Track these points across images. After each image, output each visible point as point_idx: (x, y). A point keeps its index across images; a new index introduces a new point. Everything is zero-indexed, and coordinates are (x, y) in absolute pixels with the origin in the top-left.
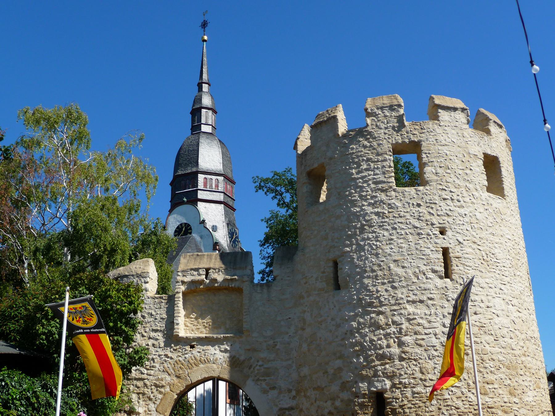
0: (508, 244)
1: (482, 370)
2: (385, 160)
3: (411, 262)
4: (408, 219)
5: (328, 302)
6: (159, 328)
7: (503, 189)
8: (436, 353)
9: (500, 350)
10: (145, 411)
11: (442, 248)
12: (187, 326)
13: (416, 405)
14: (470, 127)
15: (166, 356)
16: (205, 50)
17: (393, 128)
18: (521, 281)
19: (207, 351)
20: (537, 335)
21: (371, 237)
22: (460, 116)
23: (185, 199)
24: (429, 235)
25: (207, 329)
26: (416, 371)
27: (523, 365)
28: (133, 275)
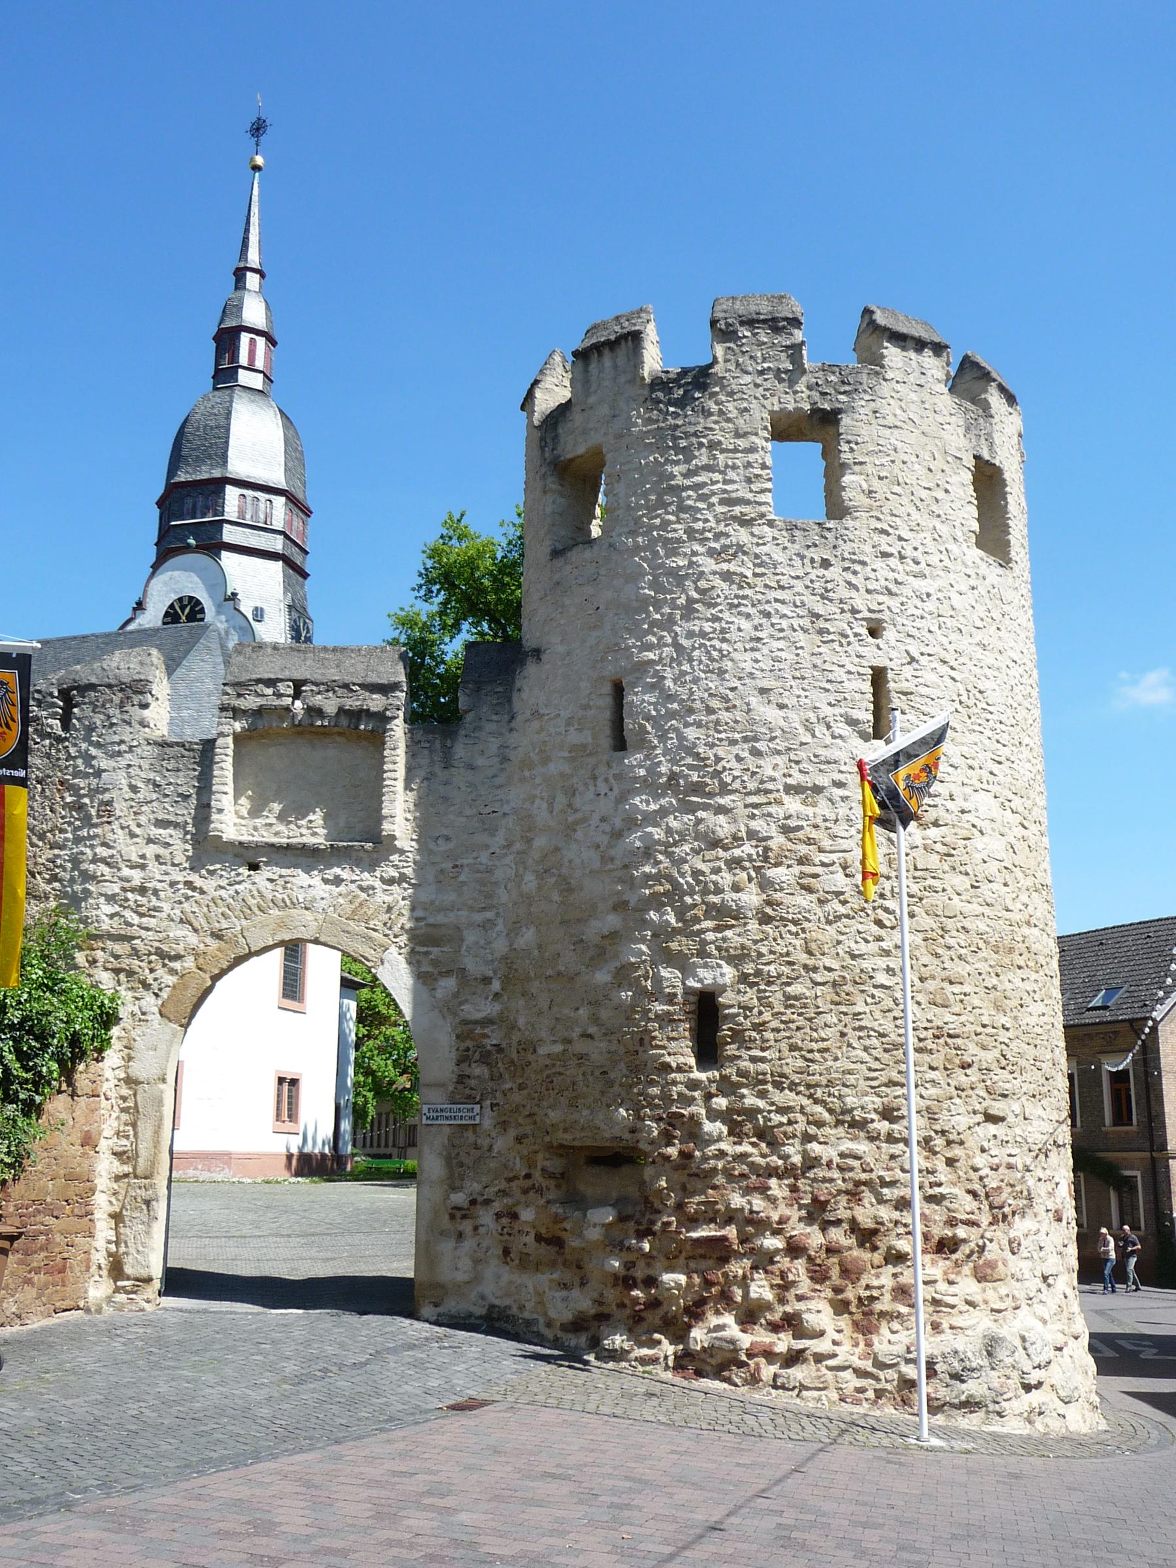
0: (1012, 672)
1: (940, 951)
2: (752, 450)
3: (799, 697)
4: (799, 594)
5: (595, 778)
8: (842, 910)
9: (980, 910)
11: (872, 668)
13: (791, 1025)
15: (189, 884)
23: (192, 541)
28: (110, 686)
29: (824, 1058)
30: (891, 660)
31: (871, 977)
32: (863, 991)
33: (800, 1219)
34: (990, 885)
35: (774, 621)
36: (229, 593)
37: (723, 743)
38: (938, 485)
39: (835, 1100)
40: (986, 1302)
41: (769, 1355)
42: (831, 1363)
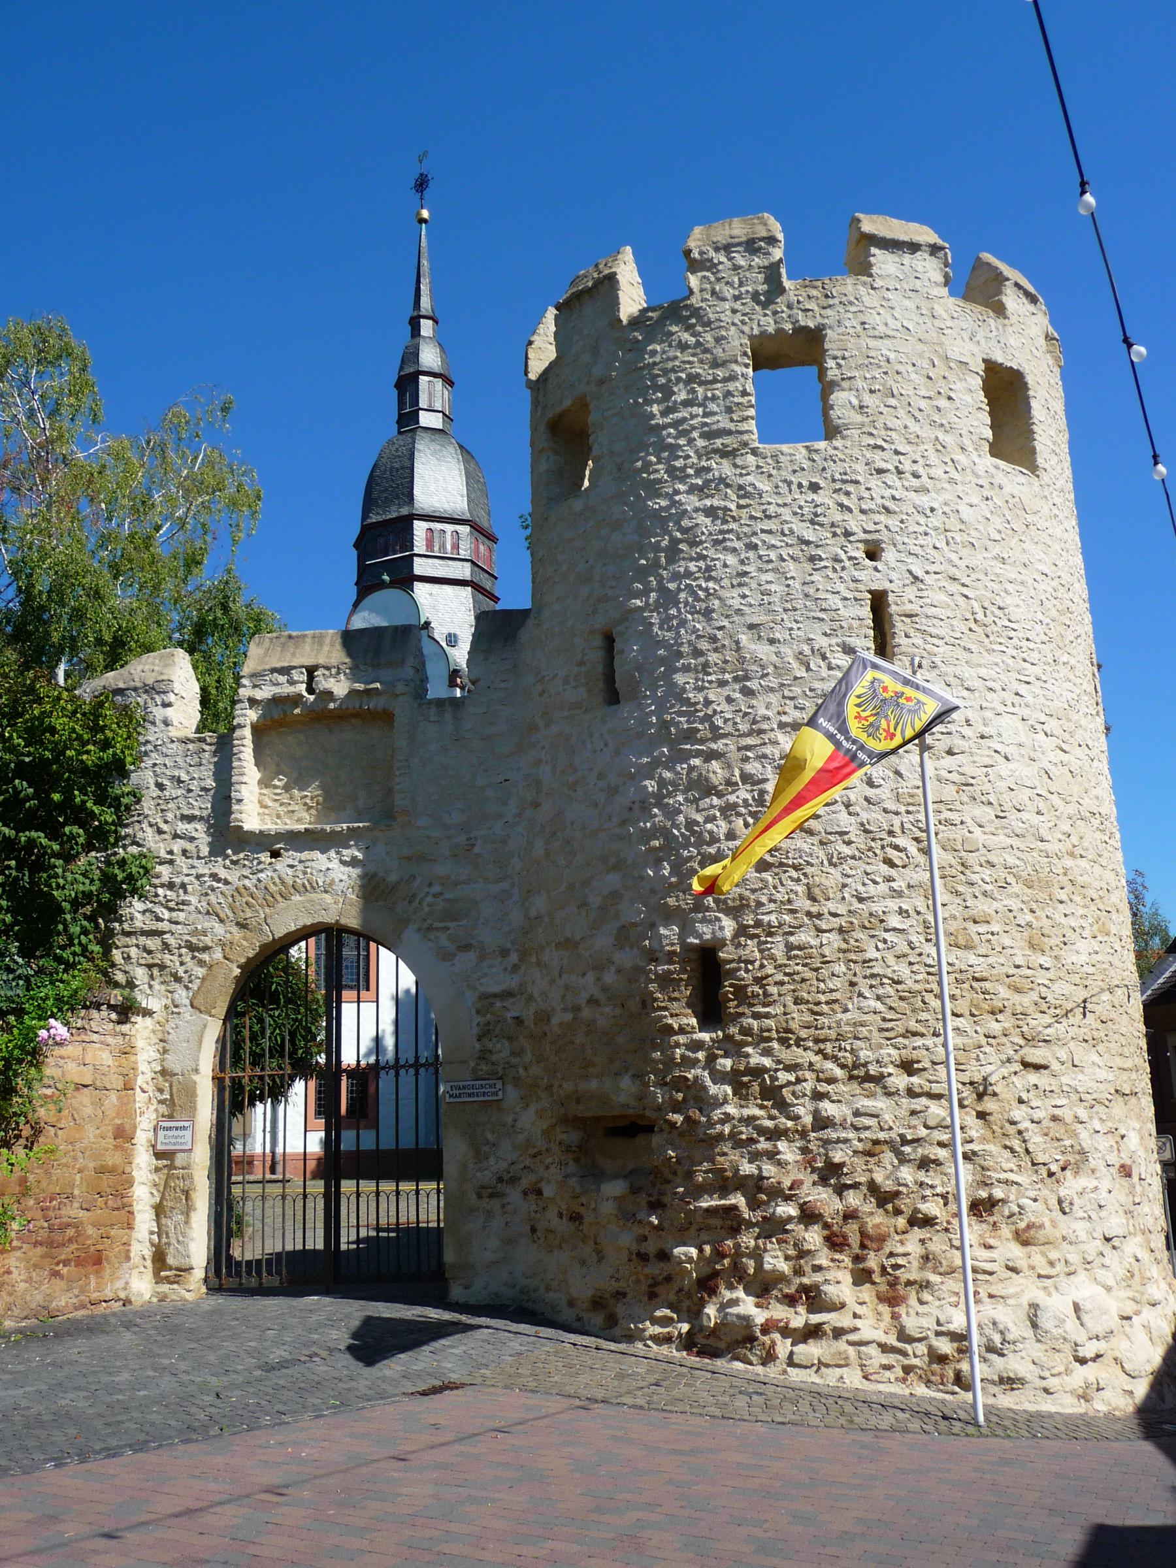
0: (1041, 586)
1: (961, 888)
2: (732, 378)
3: (791, 629)
4: (786, 522)
6: (197, 813)
7: (1033, 451)
8: (847, 851)
9: (1009, 841)
10: (166, 1007)
11: (870, 592)
12: (266, 807)
13: (795, 977)
14: (951, 294)
15: (214, 876)
16: (424, 243)
17: (755, 296)
18: (1072, 677)
19: (309, 864)
20: (1109, 808)
21: (695, 569)
22: (927, 264)
23: (386, 578)
24: (837, 560)
25: (313, 812)
26: (796, 893)
27: (1066, 878)
28: (135, 689)
29: (833, 1010)
30: (891, 582)
31: (882, 921)
32: (873, 936)
33: (814, 1184)
34: (1019, 815)
35: (761, 553)
36: (422, 622)
37: (714, 685)
38: (939, 393)
39: (848, 1055)
40: (1033, 1268)
41: (786, 1332)
42: (852, 1337)
